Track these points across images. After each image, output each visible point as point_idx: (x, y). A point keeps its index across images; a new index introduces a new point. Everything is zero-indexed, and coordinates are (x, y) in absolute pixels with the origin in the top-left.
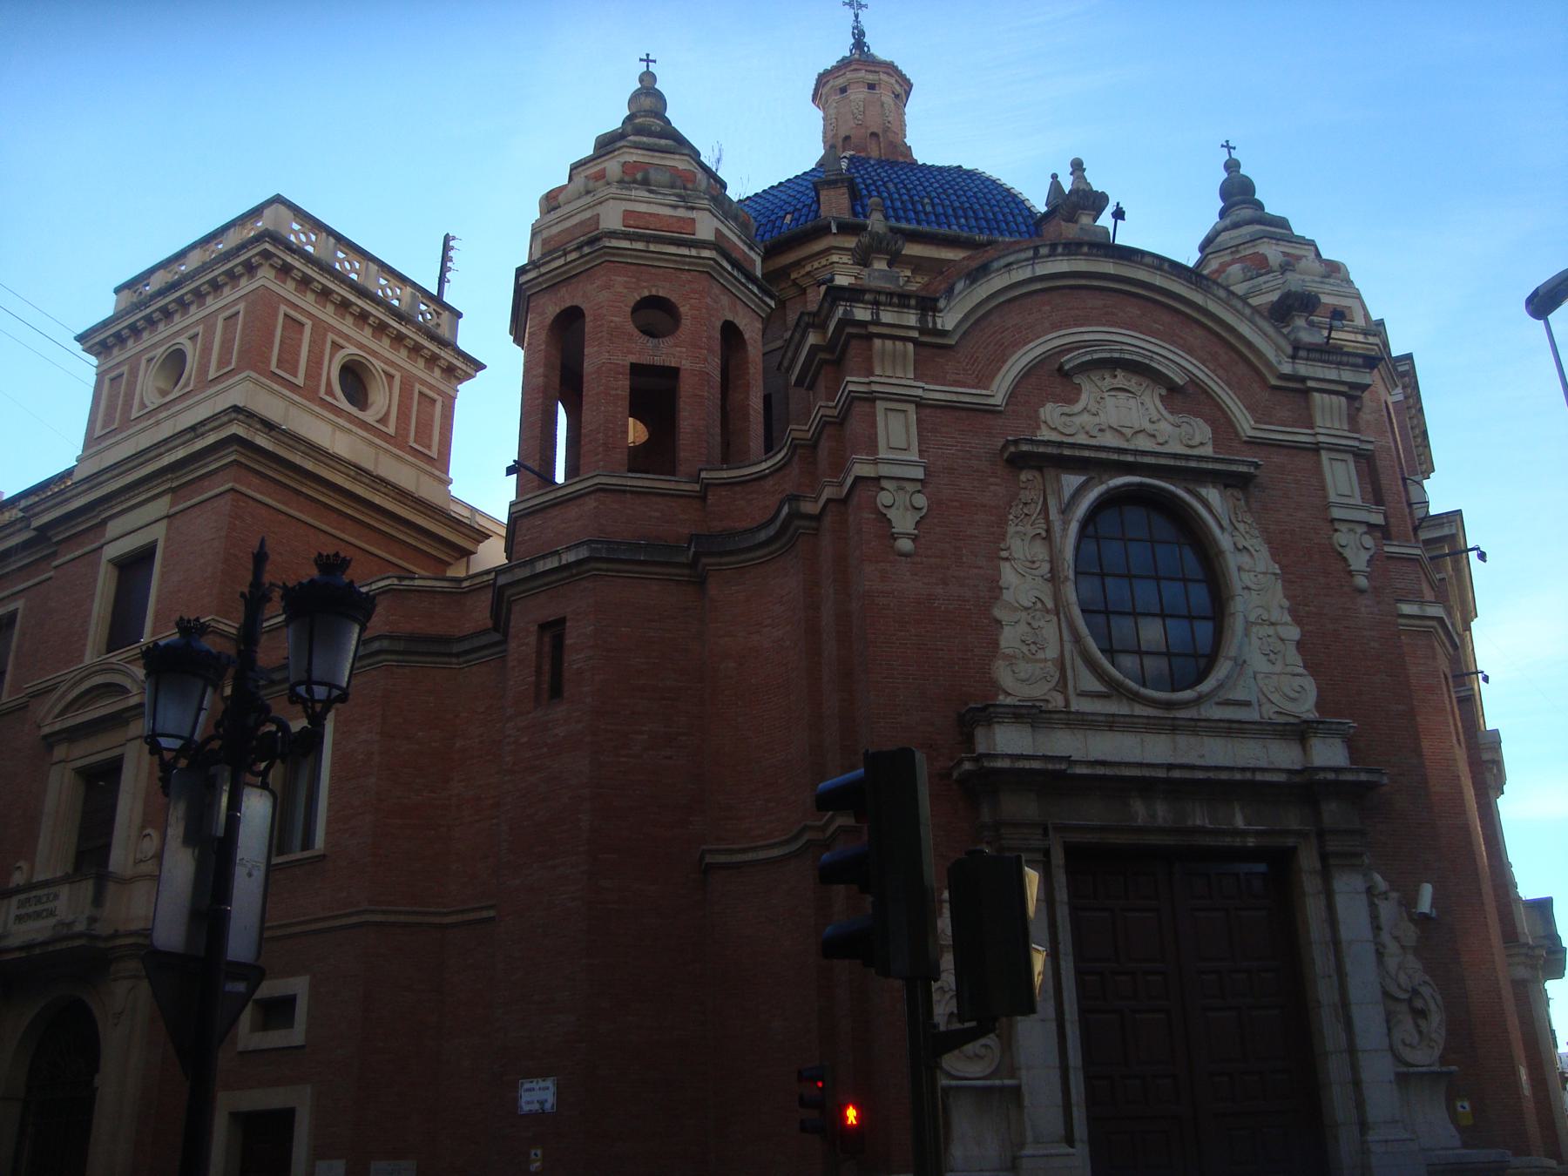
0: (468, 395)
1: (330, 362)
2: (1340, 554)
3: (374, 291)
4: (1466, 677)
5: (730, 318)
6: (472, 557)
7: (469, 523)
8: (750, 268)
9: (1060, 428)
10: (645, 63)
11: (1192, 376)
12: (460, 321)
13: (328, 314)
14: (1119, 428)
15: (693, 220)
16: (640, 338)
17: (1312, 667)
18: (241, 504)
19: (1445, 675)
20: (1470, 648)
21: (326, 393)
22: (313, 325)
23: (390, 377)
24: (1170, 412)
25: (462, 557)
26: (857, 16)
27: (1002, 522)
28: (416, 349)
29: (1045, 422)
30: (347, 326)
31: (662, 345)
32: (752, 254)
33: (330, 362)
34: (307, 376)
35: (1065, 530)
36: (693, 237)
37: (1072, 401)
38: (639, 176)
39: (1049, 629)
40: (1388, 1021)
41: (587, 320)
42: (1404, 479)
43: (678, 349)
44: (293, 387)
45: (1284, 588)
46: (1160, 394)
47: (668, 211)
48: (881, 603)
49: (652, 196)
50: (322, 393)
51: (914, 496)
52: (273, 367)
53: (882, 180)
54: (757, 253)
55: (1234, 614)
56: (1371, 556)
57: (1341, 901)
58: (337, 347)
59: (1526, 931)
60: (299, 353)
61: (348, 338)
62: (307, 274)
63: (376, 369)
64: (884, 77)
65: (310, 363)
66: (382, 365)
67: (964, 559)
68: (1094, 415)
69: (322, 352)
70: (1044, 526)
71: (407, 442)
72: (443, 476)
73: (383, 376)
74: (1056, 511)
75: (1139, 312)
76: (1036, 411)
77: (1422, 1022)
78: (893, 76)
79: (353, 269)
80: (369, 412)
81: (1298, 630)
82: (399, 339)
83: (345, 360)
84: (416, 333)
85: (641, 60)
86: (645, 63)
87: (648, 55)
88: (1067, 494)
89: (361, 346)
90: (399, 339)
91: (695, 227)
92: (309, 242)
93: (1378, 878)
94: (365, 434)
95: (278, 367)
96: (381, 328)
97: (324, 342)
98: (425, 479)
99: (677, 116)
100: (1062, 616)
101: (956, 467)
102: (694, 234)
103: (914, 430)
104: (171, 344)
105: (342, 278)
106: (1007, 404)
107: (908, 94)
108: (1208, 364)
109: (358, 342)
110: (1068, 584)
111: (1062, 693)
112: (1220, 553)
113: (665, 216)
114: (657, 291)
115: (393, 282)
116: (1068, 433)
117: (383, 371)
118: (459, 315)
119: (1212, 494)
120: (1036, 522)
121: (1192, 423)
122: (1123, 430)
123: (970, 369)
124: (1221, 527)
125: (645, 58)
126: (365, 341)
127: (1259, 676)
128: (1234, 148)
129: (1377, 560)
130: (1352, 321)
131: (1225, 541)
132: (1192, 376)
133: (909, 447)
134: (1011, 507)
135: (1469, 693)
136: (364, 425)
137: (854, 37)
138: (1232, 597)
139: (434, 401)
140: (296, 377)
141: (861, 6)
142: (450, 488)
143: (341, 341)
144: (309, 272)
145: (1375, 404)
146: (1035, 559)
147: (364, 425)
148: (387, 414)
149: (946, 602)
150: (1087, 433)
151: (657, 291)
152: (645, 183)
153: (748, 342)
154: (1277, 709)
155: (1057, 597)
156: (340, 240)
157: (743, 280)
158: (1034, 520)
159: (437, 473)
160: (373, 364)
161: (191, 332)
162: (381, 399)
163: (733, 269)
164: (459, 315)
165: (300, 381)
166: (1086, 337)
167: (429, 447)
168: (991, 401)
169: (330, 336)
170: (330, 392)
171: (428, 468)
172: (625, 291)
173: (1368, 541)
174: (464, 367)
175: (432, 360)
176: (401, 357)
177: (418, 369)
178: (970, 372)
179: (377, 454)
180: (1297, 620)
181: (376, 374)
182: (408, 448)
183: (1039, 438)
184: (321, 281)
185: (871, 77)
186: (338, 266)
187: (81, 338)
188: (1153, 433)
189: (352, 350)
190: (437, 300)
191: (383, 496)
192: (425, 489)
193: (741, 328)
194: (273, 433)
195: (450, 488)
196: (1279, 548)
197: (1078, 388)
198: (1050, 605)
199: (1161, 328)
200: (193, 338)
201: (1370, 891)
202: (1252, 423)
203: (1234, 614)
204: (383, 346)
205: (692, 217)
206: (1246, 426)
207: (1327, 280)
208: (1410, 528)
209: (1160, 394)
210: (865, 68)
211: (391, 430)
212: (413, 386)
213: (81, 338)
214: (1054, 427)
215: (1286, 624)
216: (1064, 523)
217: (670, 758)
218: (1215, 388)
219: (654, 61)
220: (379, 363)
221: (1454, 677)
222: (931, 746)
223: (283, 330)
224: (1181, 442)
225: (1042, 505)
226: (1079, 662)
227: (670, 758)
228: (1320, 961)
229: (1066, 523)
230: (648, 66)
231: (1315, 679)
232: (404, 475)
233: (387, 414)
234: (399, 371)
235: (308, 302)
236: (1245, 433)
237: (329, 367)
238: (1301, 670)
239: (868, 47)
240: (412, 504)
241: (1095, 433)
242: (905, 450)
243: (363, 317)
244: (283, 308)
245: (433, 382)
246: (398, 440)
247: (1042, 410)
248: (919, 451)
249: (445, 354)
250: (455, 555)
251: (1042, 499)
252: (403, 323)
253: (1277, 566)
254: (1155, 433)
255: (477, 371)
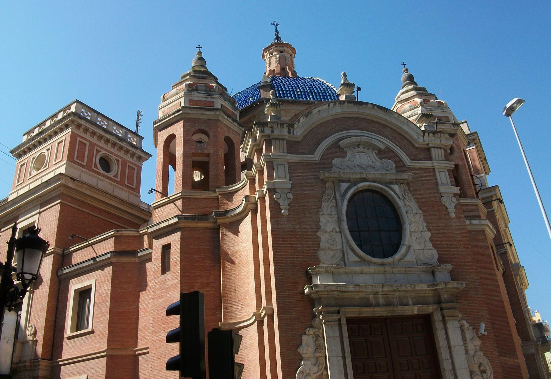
0: (146, 166)
1: (96, 156)
2: (444, 205)
3: (111, 131)
4: (504, 245)
5: (227, 134)
6: (149, 222)
7: (147, 210)
8: (234, 117)
9: (340, 167)
10: (198, 49)
11: (387, 145)
12: (143, 140)
13: (94, 140)
14: (361, 166)
15: (213, 102)
16: (198, 145)
17: (435, 246)
18: (64, 207)
19: (491, 245)
20: (509, 234)
21: (95, 167)
22: (89, 144)
23: (118, 161)
24: (379, 159)
25: (145, 222)
26: (276, 28)
27: (320, 202)
28: (127, 151)
29: (334, 165)
30: (102, 144)
31: (203, 146)
32: (235, 112)
33: (96, 156)
34: (88, 162)
35: (342, 203)
36: (213, 108)
37: (345, 157)
38: (194, 88)
39: (338, 237)
40: (471, 375)
41: (177, 138)
42: (472, 176)
43: (209, 147)
44: (82, 166)
45: (424, 218)
46: (376, 153)
47: (205, 99)
48: (308, 228)
49: (199, 94)
50: (93, 168)
51: (288, 194)
52: (75, 159)
53: (279, 84)
54: (237, 112)
55: (405, 229)
56: (456, 205)
57: (450, 331)
58: (98, 151)
59: (534, 336)
60: (84, 154)
61: (102, 148)
62: (87, 126)
63: (113, 159)
64: (286, 48)
65: (89, 157)
66: (115, 157)
67: (306, 215)
68: (352, 162)
69: (93, 153)
70: (335, 202)
71: (124, 183)
72: (138, 194)
73: (116, 161)
74: (339, 196)
75: (367, 124)
76: (331, 161)
77: (484, 375)
78: (289, 48)
79: (104, 124)
80: (111, 173)
81: (430, 233)
82: (121, 148)
83: (101, 156)
84: (127, 145)
85: (197, 48)
86: (198, 49)
87: (199, 46)
88: (343, 191)
89: (106, 150)
90: (121, 148)
91: (214, 104)
92: (88, 115)
93: (464, 322)
94: (109, 181)
95: (77, 159)
96: (114, 145)
97: (94, 150)
98: (131, 196)
99: (211, 67)
100: (342, 233)
101: (303, 183)
102: (214, 107)
103: (287, 171)
104: (41, 152)
105: (100, 127)
106: (320, 160)
107: (295, 53)
108: (393, 141)
109: (105, 150)
110: (344, 222)
111: (343, 261)
112: (399, 208)
113: (203, 101)
114: (201, 127)
115: (119, 127)
116: (342, 168)
117: (115, 159)
118: (143, 138)
119: (396, 187)
120: (332, 201)
121: (388, 162)
122: (363, 166)
123: (307, 148)
124: (399, 198)
125: (198, 47)
126: (108, 149)
127: (416, 251)
128: (406, 64)
129: (458, 206)
130: (449, 122)
131: (400, 203)
132: (387, 145)
133: (285, 177)
134: (323, 196)
135: (506, 250)
136: (108, 178)
137: (276, 36)
138: (404, 223)
139: (134, 169)
140: (83, 162)
141: (277, 25)
142: (140, 198)
143: (100, 149)
144: (87, 126)
145: (459, 150)
146: (332, 214)
147: (108, 178)
148: (117, 173)
149: (300, 231)
150: (350, 168)
151: (201, 127)
152: (196, 90)
153: (234, 143)
154: (423, 262)
155: (340, 227)
156: (98, 113)
157: (232, 122)
158: (332, 200)
159: (136, 193)
160: (111, 157)
161: (48, 148)
162: (115, 169)
163: (228, 118)
164: (143, 138)
165: (85, 164)
166: (348, 134)
167: (133, 185)
168: (314, 159)
169: (96, 148)
170: (96, 167)
171: (132, 192)
172: (190, 127)
173: (454, 200)
174: (144, 156)
175: (133, 155)
176: (122, 154)
177: (128, 158)
178: (307, 149)
179: (114, 188)
180: (429, 229)
181: (113, 161)
182: (125, 186)
183: (332, 171)
184: (92, 128)
185: (281, 49)
186: (98, 123)
187: (12, 152)
188: (373, 166)
189: (103, 152)
190: (136, 134)
191: (115, 202)
192: (132, 199)
193: (232, 138)
194: (75, 182)
195: (140, 198)
196: (422, 205)
197: (346, 153)
198: (338, 230)
199: (375, 129)
200: (48, 150)
201: (461, 327)
202: (409, 160)
203: (405, 229)
204: (115, 151)
205: (213, 100)
206: (407, 161)
207: (439, 108)
208: (475, 193)
209: (376, 153)
210: (279, 45)
211: (119, 179)
212: (126, 163)
213: (12, 152)
214: (337, 166)
215: (425, 231)
216: (342, 200)
217: (208, 291)
218: (396, 149)
219: (201, 48)
220: (113, 155)
221: (496, 246)
222: (296, 283)
223: (78, 146)
224: (384, 169)
225: (334, 194)
226: (349, 250)
227: (208, 291)
228: (444, 354)
229: (343, 200)
230: (199, 50)
231: (437, 251)
232: (123, 194)
233: (117, 173)
234: (121, 159)
235: (88, 136)
236: (407, 164)
237: (96, 158)
238: (432, 248)
239: (281, 38)
240: (126, 205)
241: (353, 168)
242: (284, 178)
243: (108, 141)
244: (79, 139)
245: (133, 162)
246: (121, 183)
247: (333, 161)
248: (289, 178)
249: (138, 152)
250: (143, 222)
251: (334, 192)
252: (122, 142)
253: (421, 211)
254: (375, 167)
255: (149, 157)
